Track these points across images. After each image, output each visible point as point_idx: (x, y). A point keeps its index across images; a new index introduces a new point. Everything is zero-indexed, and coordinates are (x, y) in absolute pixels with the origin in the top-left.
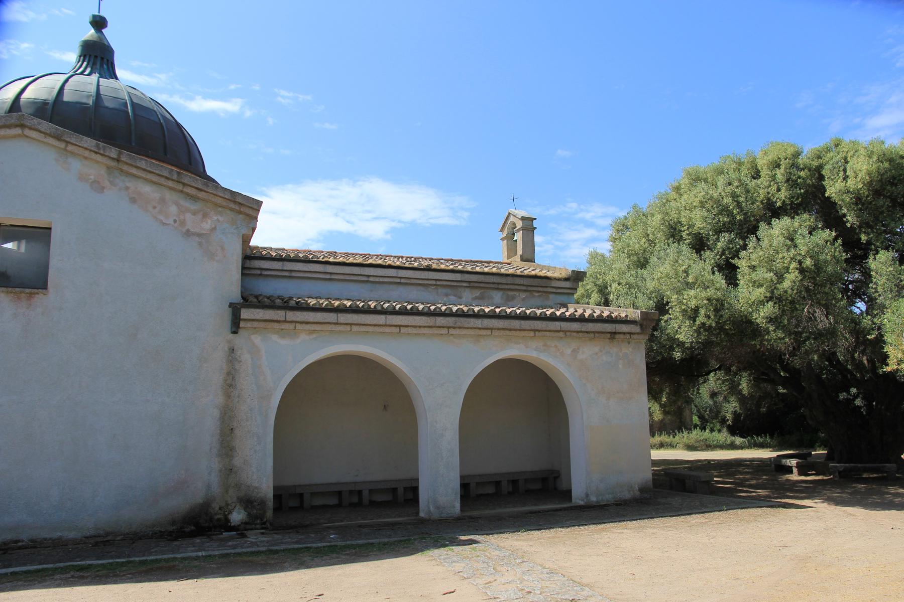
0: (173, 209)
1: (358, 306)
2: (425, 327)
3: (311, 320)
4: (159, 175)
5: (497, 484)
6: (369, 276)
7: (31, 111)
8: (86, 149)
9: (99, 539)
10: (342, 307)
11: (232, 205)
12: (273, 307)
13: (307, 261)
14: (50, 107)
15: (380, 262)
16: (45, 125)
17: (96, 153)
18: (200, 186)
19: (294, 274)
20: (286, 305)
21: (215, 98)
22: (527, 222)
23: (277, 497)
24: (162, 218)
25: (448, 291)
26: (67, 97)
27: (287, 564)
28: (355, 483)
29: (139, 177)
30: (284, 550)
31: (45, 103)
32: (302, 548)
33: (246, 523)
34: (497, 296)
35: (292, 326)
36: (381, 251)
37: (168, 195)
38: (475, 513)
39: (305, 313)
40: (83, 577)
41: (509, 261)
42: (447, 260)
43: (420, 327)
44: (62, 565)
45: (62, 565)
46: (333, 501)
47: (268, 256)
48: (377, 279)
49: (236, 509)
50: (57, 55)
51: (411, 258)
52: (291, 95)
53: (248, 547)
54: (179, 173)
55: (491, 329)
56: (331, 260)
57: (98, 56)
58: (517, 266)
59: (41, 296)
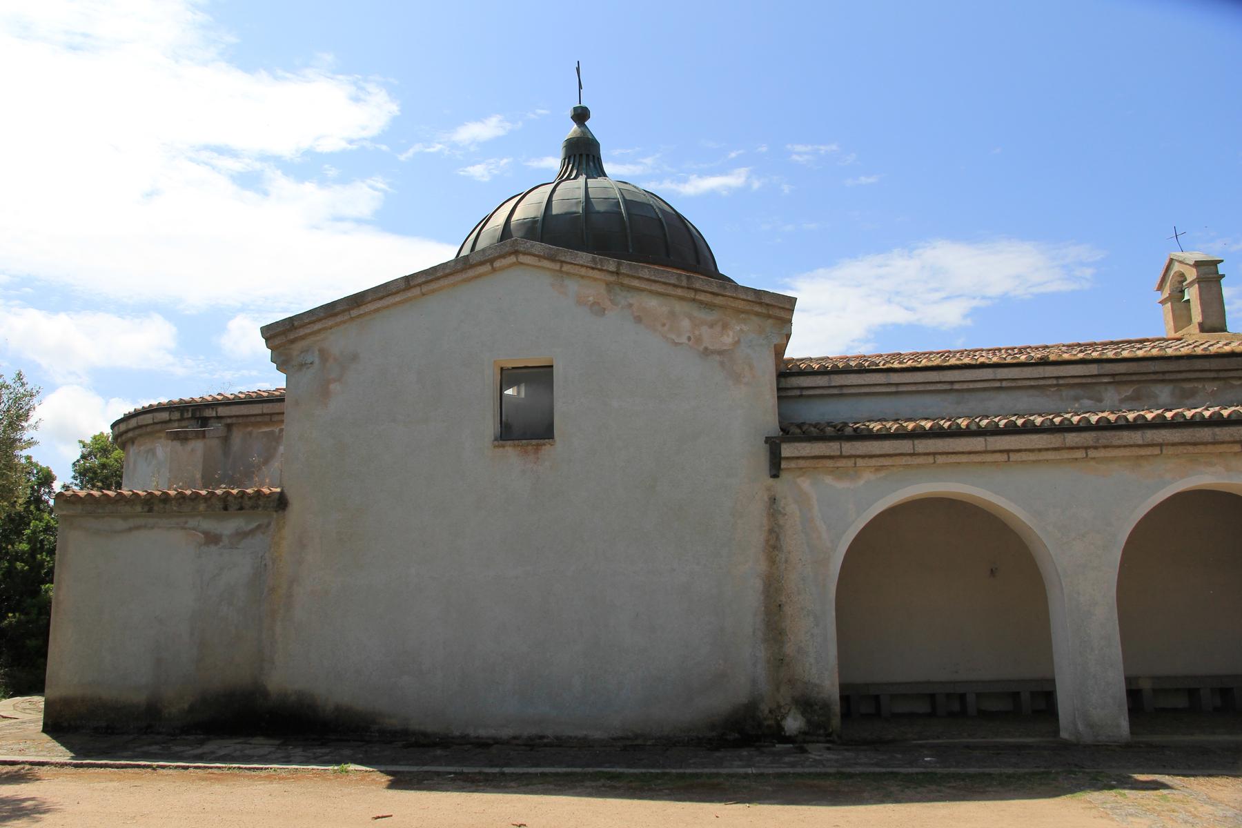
0: (686, 323)
1: (941, 427)
2: (1047, 450)
3: (878, 452)
4: (665, 283)
5: (1192, 693)
6: (952, 383)
7: (521, 234)
8: (582, 266)
9: (629, 743)
10: (918, 431)
11: (757, 309)
12: (822, 438)
13: (861, 370)
14: (539, 225)
15: (967, 361)
16: (539, 247)
17: (593, 268)
18: (715, 290)
19: (845, 391)
20: (840, 433)
21: (711, 173)
22: (1205, 269)
23: (845, 699)
24: (673, 337)
25: (1080, 392)
26: (556, 210)
27: (865, 795)
28: (955, 683)
29: (642, 290)
30: (860, 775)
31: (534, 221)
32: (885, 774)
33: (805, 733)
34: (1164, 393)
35: (850, 463)
36: (958, 345)
37: (679, 307)
38: (1156, 739)
39: (867, 443)
40: (614, 788)
41: (1178, 335)
42: (1071, 347)
43: (1040, 450)
44: (590, 770)
45: (590, 770)
46: (923, 708)
47: (809, 370)
48: (965, 386)
49: (793, 711)
50: (535, 164)
51: (1013, 349)
52: (809, 148)
53: (811, 766)
54: (688, 278)
55: (1161, 445)
56: (896, 365)
57: (583, 154)
58: (1195, 341)
59: (547, 447)
